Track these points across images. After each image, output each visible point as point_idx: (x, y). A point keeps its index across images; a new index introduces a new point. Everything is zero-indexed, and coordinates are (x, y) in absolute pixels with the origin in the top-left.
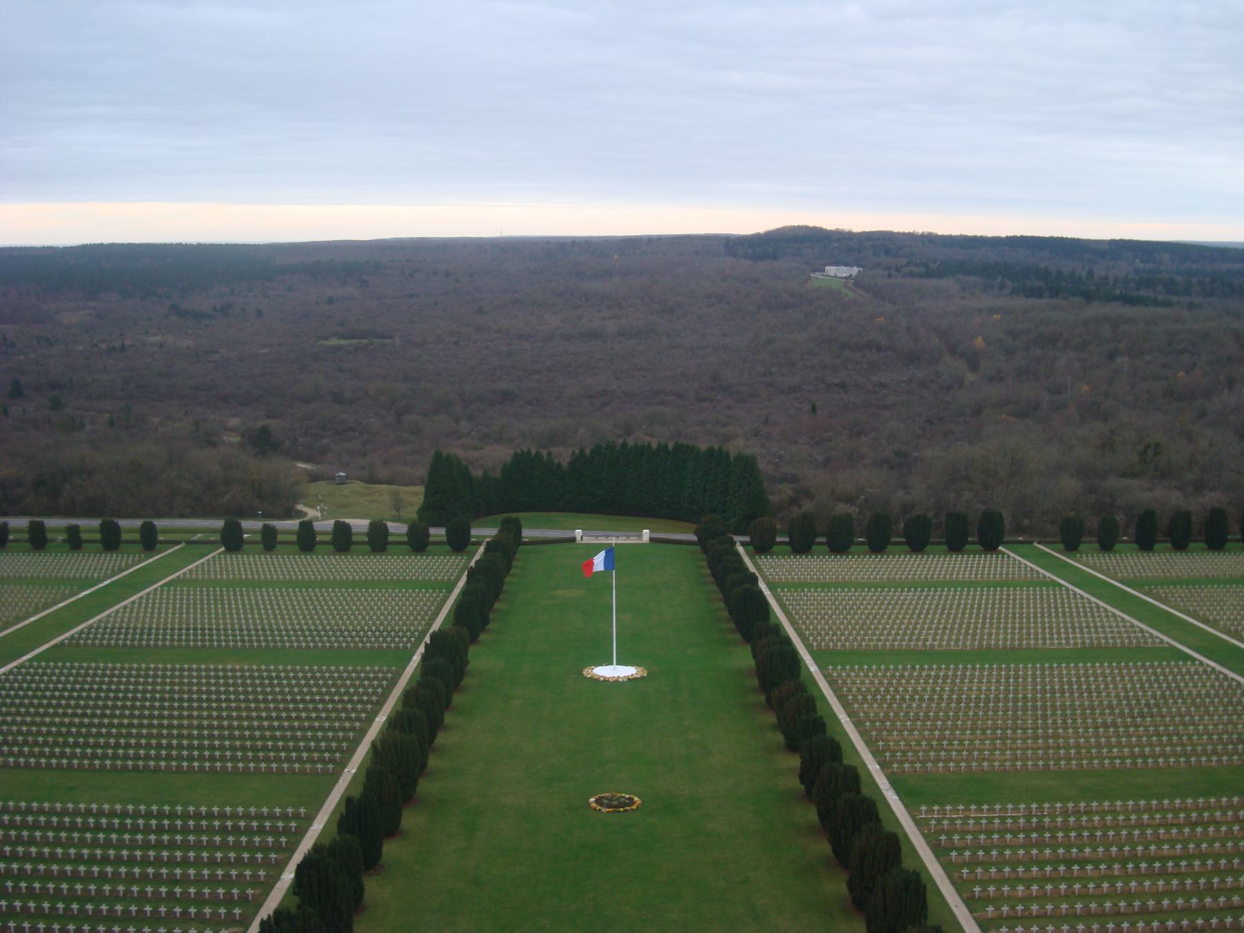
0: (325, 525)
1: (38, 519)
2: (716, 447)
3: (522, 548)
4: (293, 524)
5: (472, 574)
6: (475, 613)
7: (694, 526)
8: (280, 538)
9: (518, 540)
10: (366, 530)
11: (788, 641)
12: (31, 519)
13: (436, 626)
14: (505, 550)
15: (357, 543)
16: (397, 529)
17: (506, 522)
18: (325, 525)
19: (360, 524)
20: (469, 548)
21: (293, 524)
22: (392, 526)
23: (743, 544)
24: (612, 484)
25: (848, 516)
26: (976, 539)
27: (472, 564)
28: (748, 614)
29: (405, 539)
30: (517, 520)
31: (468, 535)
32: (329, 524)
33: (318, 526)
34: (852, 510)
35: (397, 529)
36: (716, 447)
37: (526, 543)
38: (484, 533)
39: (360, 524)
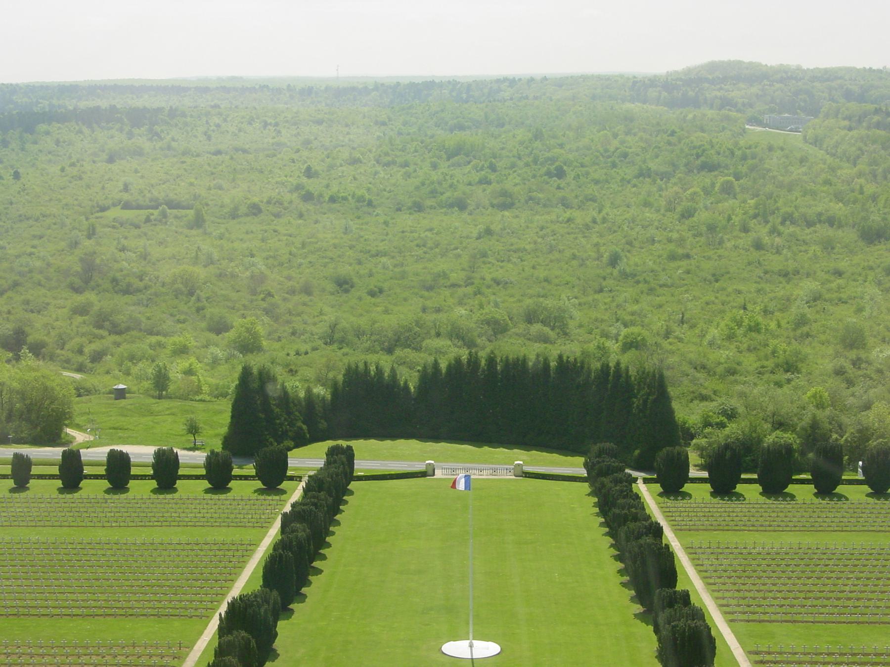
0: (95, 454)
1: (343, 443)
2: (465, 358)
3: (353, 485)
4: (55, 453)
5: (287, 520)
6: (291, 569)
7: (581, 460)
8: (35, 470)
9: (350, 476)
10: (151, 460)
11: (699, 615)
12: (330, 443)
13: (236, 591)
14: (332, 490)
15: (137, 477)
16: (192, 459)
17: (332, 453)
18: (95, 454)
19: (142, 453)
20: (285, 485)
21: (55, 453)
22: (183, 455)
23: (646, 481)
24: (490, 403)
25: (789, 449)
26: (860, 476)
27: (288, 509)
28: (650, 574)
29: (203, 472)
30: (350, 448)
31: (283, 465)
32: (101, 453)
33: (86, 455)
34: (788, 437)
35: (192, 459)
36: (465, 358)
37: (360, 478)
38: (306, 461)
39: (142, 453)
